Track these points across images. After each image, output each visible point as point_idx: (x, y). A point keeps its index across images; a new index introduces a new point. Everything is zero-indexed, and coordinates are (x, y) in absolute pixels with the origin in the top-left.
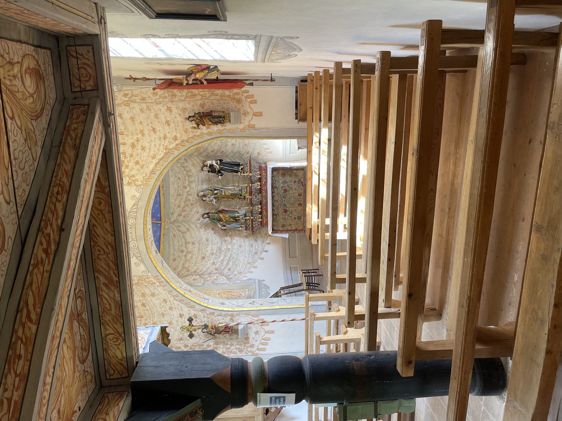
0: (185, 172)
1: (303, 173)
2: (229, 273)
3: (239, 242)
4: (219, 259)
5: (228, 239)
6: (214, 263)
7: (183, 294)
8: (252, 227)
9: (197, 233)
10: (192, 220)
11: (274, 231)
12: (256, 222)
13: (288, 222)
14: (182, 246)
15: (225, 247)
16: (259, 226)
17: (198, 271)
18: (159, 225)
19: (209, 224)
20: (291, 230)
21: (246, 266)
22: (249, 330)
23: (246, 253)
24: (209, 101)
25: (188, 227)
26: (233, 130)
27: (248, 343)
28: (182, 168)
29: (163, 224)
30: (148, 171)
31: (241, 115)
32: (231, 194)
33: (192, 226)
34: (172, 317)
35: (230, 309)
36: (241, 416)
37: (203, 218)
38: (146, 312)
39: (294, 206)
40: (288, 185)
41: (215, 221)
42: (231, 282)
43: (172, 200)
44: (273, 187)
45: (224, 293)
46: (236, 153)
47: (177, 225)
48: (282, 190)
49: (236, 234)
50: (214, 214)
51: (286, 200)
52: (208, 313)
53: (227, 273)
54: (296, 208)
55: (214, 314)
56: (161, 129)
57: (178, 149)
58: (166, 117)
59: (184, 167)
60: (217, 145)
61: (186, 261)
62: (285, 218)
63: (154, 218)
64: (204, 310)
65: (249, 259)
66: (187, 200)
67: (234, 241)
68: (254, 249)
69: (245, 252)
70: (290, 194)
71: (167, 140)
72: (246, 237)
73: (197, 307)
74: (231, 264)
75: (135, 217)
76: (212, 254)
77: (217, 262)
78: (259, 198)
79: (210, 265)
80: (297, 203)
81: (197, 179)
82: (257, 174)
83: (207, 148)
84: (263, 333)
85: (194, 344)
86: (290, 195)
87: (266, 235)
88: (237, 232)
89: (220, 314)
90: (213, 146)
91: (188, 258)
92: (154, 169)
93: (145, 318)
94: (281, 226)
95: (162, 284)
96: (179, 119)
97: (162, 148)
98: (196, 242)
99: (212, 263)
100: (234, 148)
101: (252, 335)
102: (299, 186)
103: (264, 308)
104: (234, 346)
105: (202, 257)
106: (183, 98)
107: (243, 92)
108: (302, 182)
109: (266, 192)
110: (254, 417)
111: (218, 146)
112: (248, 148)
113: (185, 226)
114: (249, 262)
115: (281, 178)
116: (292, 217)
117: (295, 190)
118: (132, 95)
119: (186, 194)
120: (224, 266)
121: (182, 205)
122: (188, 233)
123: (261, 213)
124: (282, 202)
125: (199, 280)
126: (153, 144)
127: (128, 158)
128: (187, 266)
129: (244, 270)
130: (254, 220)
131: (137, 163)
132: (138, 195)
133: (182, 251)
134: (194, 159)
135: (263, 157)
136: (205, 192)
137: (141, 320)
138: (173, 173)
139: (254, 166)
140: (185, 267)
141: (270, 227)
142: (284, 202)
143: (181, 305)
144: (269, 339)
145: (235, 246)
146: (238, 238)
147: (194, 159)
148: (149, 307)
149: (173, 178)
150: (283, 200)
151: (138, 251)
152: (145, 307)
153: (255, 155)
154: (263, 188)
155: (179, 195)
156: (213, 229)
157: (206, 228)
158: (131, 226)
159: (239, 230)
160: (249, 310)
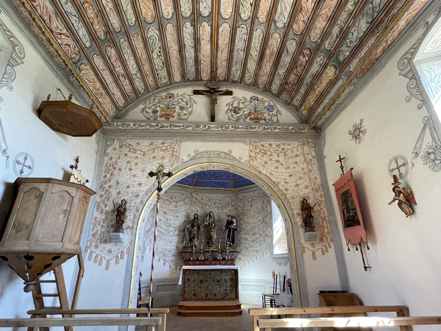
0: (225, 205)
1: (233, 297)
4: (163, 224)
5: (177, 233)
6: (161, 221)
8: (185, 252)
9: (183, 210)
12: (189, 256)
14: (175, 198)
15: (171, 230)
20: (184, 287)
22: (114, 243)
24: (317, 216)
25: (188, 204)
26: (298, 234)
27: (100, 243)
28: (227, 203)
29: (192, 187)
30: (261, 169)
31: (312, 241)
33: (188, 207)
34: (140, 177)
35: (139, 226)
36: (35, 223)
38: (148, 159)
40: (224, 283)
41: (192, 223)
43: (207, 195)
44: (222, 270)
46: (240, 241)
47: (190, 197)
49: (180, 239)
51: (211, 282)
54: (203, 291)
55: (137, 211)
56: (292, 180)
57: (279, 191)
58: (301, 184)
59: (228, 204)
60: (246, 227)
61: (165, 200)
64: (142, 204)
65: (160, 249)
66: (206, 205)
69: (166, 246)
71: (284, 184)
72: (177, 247)
73: (146, 198)
76: (167, 220)
77: (161, 223)
78: (209, 258)
80: (208, 293)
83: (243, 220)
84: (108, 258)
85: (110, 193)
86: (215, 286)
88: (181, 240)
89: (135, 217)
91: (167, 202)
92: (262, 173)
93: (143, 157)
96: (301, 193)
97: (278, 180)
98: (177, 208)
101: (108, 246)
103: (134, 259)
104: (100, 229)
106: (316, 196)
107: (329, 243)
108: (225, 297)
109: (215, 264)
110: (28, 239)
113: (188, 202)
114: (158, 249)
115: (229, 277)
117: (220, 291)
118: (312, 164)
119: (210, 204)
121: (203, 201)
122: (183, 203)
123: (198, 260)
124: (209, 278)
126: (281, 174)
127: (268, 158)
130: (191, 254)
131: (266, 163)
132: (243, 161)
133: (171, 198)
136: (213, 217)
137: (141, 154)
139: (233, 255)
141: (188, 268)
142: (209, 280)
143: (150, 185)
144: (100, 264)
146: (176, 241)
148: (152, 161)
150: (211, 280)
152: (153, 158)
153: (239, 256)
154: (218, 262)
155: (210, 200)
156: (185, 221)
158: (220, 154)
159: (183, 241)
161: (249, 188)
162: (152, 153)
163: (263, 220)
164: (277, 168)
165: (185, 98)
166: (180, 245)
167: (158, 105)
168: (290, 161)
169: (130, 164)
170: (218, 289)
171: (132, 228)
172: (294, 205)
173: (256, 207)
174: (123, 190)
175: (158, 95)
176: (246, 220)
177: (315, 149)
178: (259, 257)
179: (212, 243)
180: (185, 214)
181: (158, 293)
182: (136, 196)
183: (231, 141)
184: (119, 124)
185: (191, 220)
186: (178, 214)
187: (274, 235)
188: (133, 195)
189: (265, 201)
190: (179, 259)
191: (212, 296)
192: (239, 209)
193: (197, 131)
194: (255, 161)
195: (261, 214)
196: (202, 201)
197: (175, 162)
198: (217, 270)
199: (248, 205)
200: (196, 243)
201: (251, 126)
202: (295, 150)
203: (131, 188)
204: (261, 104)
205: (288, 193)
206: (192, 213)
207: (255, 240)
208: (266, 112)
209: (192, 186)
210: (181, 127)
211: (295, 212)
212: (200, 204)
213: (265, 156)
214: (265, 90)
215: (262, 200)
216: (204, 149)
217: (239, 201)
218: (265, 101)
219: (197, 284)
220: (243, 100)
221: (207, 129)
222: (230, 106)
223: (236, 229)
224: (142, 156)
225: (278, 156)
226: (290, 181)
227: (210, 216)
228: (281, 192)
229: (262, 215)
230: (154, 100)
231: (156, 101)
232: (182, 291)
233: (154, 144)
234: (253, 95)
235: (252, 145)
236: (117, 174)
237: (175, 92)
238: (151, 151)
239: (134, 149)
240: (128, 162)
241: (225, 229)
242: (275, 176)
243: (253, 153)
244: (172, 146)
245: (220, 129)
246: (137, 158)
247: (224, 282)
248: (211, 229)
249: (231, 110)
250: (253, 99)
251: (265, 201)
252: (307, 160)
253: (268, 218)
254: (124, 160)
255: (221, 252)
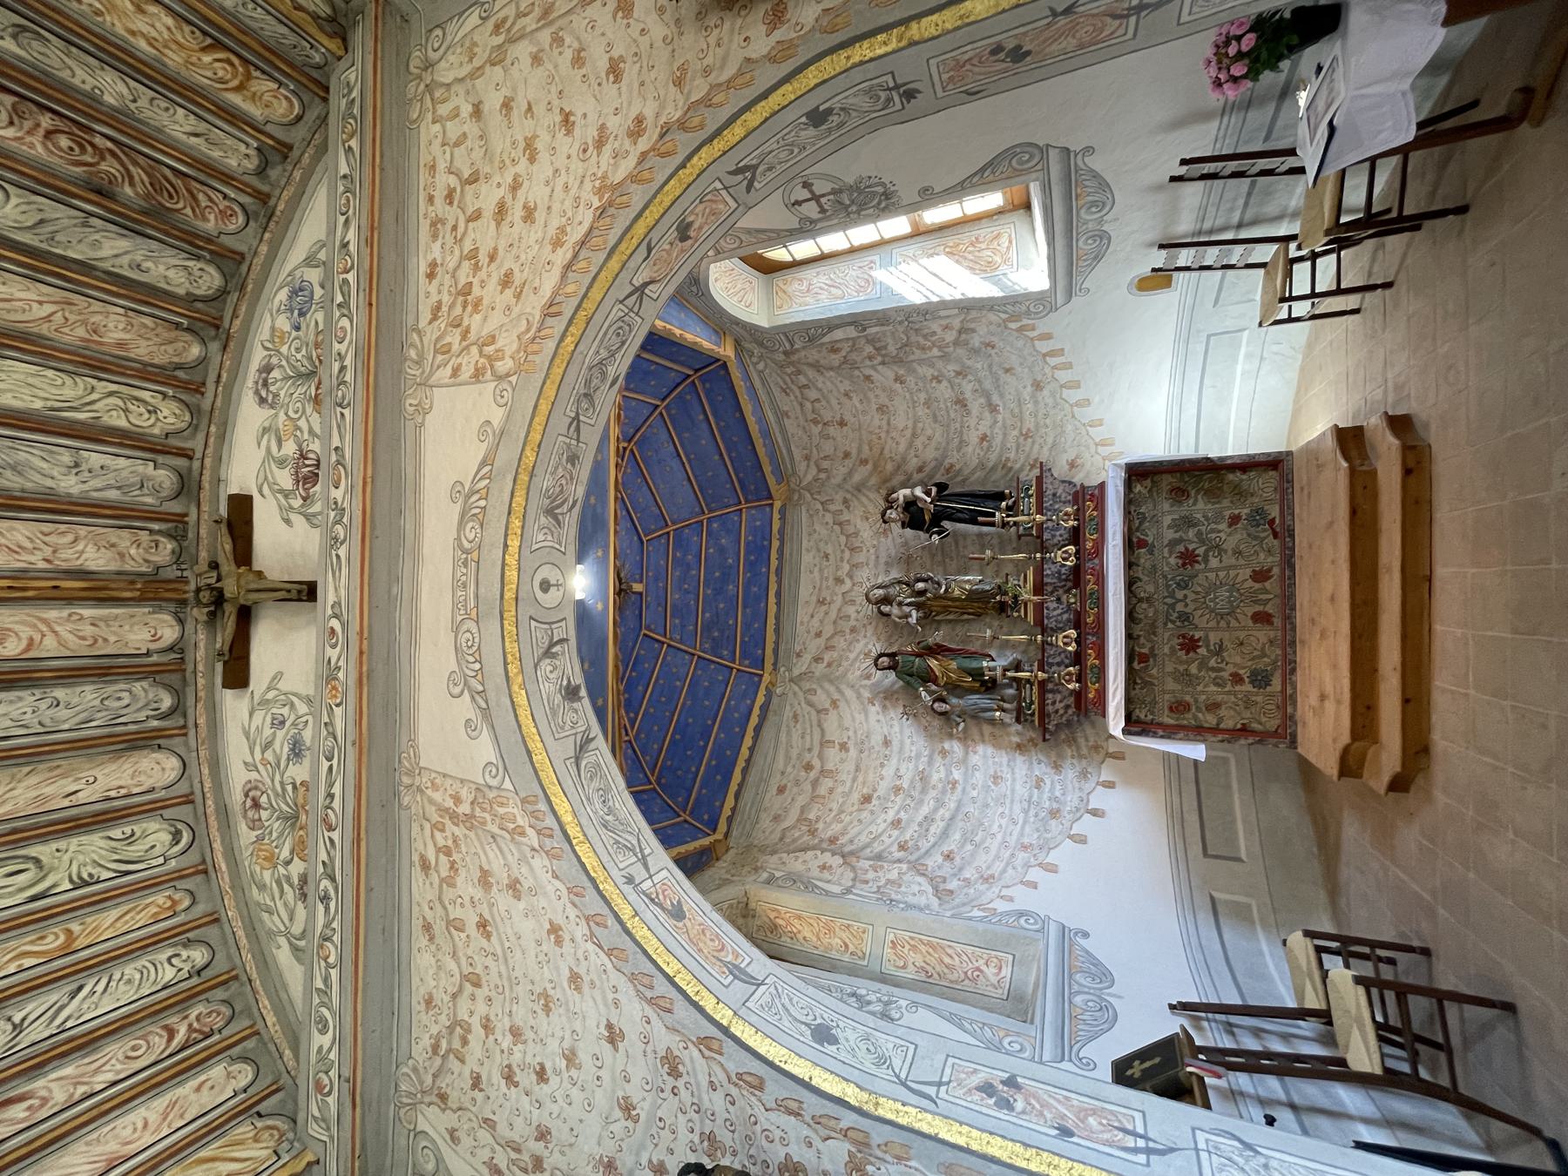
0: (843, 539)
1: (1274, 483)
2: (947, 870)
3: (990, 762)
4: (917, 810)
5: (955, 747)
6: (899, 821)
7: (625, 918)
8: (1043, 714)
9: (860, 717)
10: (850, 676)
11: (1134, 724)
12: (1059, 697)
13: (1203, 692)
14: (810, 750)
15: (942, 775)
16: (1070, 712)
17: (843, 840)
18: (756, 679)
19: (896, 692)
21: (1013, 855)
23: (1017, 808)
25: (836, 696)
28: (837, 528)
29: (766, 678)
30: (533, 305)
32: (970, 591)
33: (849, 693)
34: (578, 1026)
35: (852, 1094)
37: (876, 665)
38: (489, 961)
39: (1234, 623)
40: (1199, 533)
42: (946, 906)
43: (802, 614)
44: (1132, 544)
45: (914, 948)
46: (994, 469)
47: (807, 685)
48: (1171, 553)
49: (982, 735)
50: (912, 658)
51: (1191, 596)
52: (732, 1068)
53: (939, 867)
54: (1242, 635)
56: (590, 106)
57: (646, 175)
59: (840, 524)
60: (933, 444)
61: (813, 798)
62: (1187, 673)
63: (745, 658)
65: (1027, 829)
67: (975, 759)
68: (1046, 796)
69: (1012, 801)
70: (1211, 570)
71: (607, 150)
72: (1019, 747)
73: (682, 1010)
74: (957, 836)
75: (480, 516)
76: (897, 790)
77: (910, 820)
78: (1069, 604)
79: (883, 826)
80: (1250, 611)
81: (873, 557)
82: (1066, 514)
83: (904, 459)
86: (1212, 576)
87: (1098, 753)
88: (987, 729)
90: (920, 447)
91: (822, 790)
92: (555, 293)
94: (1166, 704)
95: (548, 843)
96: (658, 30)
98: (851, 745)
99: (892, 823)
100: (988, 450)
102: (1256, 538)
105: (863, 796)
108: (1272, 522)
109: (1101, 579)
111: (937, 449)
112: (1036, 447)
114: (1026, 840)
115: (1166, 506)
116: (1221, 670)
117: (1238, 553)
119: (839, 599)
120: (932, 840)
121: (828, 630)
122: (833, 715)
123: (1078, 658)
124: (1172, 606)
125: (840, 871)
126: (560, 182)
128: (812, 816)
129: (1004, 871)
130: (1050, 686)
131: (506, 282)
132: (497, 416)
134: (867, 497)
135: (1087, 476)
137: (473, 998)
138: (812, 543)
139: (1054, 495)
140: (805, 819)
141: (1117, 709)
142: (1180, 607)
143: (616, 978)
145: (977, 774)
146: (990, 750)
147: (867, 497)
148: (502, 945)
149: (811, 554)
150: (1180, 594)
151: (477, 666)
152: (488, 936)
153: (1060, 469)
157: (888, 703)
159: (992, 721)
160: (967, 1151)
161: (766, 433)
162: (463, 935)
163: (898, 361)
164: (529, 215)
165: (259, 730)
166: (1008, 734)
167: (282, 870)
168: (499, 144)
169: (517, 1070)
170: (1229, 560)
171: (863, 1144)
172: (725, 59)
173: (844, 400)
174: (642, 1147)
175: (246, 864)
176: (902, 448)
177: (451, 19)
178: (1063, 376)
179: (1000, 590)
180: (877, 707)
181: (1244, 857)
182: (674, 1073)
183: (417, 490)
184: (317, 1114)
185: (901, 683)
186: (877, 739)
187: (958, 296)
188: (668, 1088)
189: (813, 355)
190: (1075, 740)
191: (1267, 592)
192: (857, 478)
193: (352, 682)
194: (499, 345)
195: (872, 372)
196: (826, 635)
197: (501, 811)
198: (1130, 565)
199: (839, 439)
200: (1001, 663)
201: (335, 382)
202: (453, 130)
203: (635, 1092)
204: (284, 349)
205: (657, 115)
206: (874, 680)
207: (988, 396)
208: (313, 323)
209: (761, 676)
210: (331, 768)
211: (762, 44)
212: (840, 643)
213: (476, 291)
214: (213, 332)
215: (811, 373)
216: (447, 639)
217: (828, 478)
218: (273, 329)
219: (1203, 665)
220: (269, 441)
221: (343, 625)
222: (291, 507)
223: (942, 487)
224: (481, 993)
225: (476, 216)
226: (592, 117)
227: (887, 600)
228: (653, 160)
229: (873, 367)
230: (262, 887)
231: (267, 875)
232: (1243, 742)
233: (429, 915)
234: (251, 393)
235: (431, 374)
236: (562, 1153)
237: (238, 777)
238: (457, 939)
239: (451, 1029)
240: (509, 1078)
241: (939, 533)
242: (570, 214)
243: (464, 360)
244: (435, 818)
245: (342, 552)
246: (487, 1027)
247: (1191, 533)
248: (937, 597)
249: (305, 499)
250: (264, 394)
251: (813, 355)
252: (500, 46)
253: (884, 333)
254: (501, 1100)
255: (1043, 549)
